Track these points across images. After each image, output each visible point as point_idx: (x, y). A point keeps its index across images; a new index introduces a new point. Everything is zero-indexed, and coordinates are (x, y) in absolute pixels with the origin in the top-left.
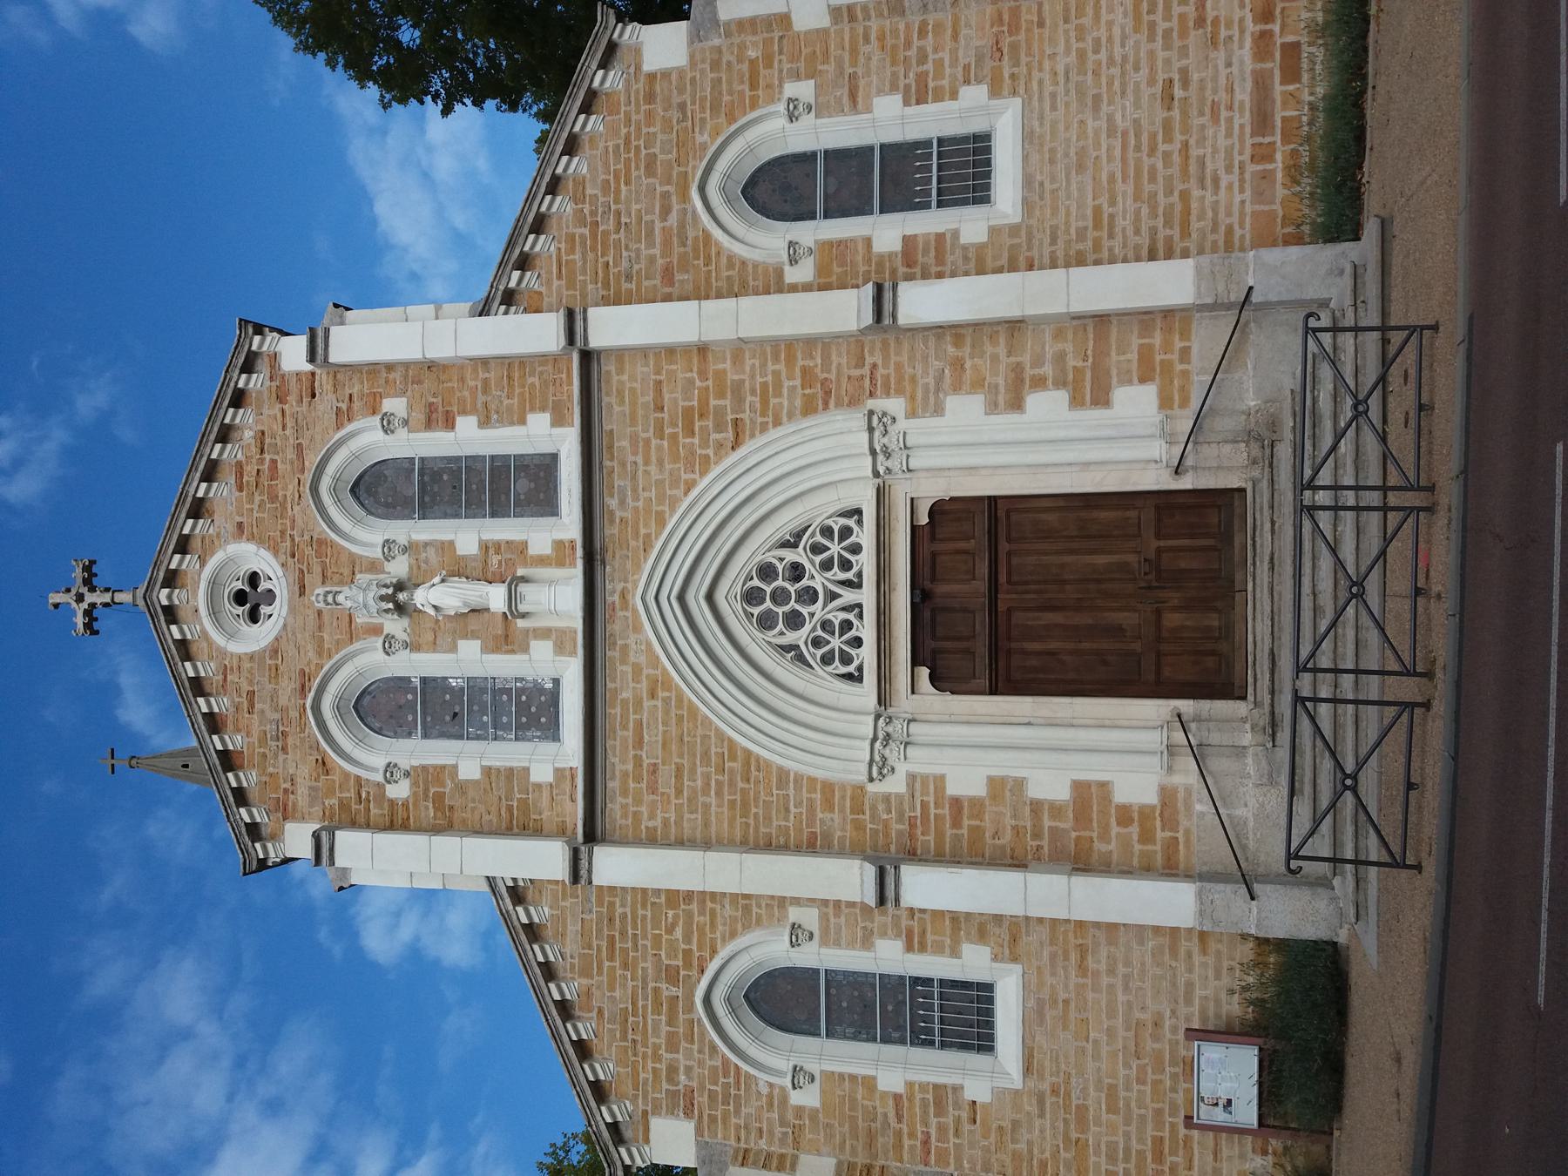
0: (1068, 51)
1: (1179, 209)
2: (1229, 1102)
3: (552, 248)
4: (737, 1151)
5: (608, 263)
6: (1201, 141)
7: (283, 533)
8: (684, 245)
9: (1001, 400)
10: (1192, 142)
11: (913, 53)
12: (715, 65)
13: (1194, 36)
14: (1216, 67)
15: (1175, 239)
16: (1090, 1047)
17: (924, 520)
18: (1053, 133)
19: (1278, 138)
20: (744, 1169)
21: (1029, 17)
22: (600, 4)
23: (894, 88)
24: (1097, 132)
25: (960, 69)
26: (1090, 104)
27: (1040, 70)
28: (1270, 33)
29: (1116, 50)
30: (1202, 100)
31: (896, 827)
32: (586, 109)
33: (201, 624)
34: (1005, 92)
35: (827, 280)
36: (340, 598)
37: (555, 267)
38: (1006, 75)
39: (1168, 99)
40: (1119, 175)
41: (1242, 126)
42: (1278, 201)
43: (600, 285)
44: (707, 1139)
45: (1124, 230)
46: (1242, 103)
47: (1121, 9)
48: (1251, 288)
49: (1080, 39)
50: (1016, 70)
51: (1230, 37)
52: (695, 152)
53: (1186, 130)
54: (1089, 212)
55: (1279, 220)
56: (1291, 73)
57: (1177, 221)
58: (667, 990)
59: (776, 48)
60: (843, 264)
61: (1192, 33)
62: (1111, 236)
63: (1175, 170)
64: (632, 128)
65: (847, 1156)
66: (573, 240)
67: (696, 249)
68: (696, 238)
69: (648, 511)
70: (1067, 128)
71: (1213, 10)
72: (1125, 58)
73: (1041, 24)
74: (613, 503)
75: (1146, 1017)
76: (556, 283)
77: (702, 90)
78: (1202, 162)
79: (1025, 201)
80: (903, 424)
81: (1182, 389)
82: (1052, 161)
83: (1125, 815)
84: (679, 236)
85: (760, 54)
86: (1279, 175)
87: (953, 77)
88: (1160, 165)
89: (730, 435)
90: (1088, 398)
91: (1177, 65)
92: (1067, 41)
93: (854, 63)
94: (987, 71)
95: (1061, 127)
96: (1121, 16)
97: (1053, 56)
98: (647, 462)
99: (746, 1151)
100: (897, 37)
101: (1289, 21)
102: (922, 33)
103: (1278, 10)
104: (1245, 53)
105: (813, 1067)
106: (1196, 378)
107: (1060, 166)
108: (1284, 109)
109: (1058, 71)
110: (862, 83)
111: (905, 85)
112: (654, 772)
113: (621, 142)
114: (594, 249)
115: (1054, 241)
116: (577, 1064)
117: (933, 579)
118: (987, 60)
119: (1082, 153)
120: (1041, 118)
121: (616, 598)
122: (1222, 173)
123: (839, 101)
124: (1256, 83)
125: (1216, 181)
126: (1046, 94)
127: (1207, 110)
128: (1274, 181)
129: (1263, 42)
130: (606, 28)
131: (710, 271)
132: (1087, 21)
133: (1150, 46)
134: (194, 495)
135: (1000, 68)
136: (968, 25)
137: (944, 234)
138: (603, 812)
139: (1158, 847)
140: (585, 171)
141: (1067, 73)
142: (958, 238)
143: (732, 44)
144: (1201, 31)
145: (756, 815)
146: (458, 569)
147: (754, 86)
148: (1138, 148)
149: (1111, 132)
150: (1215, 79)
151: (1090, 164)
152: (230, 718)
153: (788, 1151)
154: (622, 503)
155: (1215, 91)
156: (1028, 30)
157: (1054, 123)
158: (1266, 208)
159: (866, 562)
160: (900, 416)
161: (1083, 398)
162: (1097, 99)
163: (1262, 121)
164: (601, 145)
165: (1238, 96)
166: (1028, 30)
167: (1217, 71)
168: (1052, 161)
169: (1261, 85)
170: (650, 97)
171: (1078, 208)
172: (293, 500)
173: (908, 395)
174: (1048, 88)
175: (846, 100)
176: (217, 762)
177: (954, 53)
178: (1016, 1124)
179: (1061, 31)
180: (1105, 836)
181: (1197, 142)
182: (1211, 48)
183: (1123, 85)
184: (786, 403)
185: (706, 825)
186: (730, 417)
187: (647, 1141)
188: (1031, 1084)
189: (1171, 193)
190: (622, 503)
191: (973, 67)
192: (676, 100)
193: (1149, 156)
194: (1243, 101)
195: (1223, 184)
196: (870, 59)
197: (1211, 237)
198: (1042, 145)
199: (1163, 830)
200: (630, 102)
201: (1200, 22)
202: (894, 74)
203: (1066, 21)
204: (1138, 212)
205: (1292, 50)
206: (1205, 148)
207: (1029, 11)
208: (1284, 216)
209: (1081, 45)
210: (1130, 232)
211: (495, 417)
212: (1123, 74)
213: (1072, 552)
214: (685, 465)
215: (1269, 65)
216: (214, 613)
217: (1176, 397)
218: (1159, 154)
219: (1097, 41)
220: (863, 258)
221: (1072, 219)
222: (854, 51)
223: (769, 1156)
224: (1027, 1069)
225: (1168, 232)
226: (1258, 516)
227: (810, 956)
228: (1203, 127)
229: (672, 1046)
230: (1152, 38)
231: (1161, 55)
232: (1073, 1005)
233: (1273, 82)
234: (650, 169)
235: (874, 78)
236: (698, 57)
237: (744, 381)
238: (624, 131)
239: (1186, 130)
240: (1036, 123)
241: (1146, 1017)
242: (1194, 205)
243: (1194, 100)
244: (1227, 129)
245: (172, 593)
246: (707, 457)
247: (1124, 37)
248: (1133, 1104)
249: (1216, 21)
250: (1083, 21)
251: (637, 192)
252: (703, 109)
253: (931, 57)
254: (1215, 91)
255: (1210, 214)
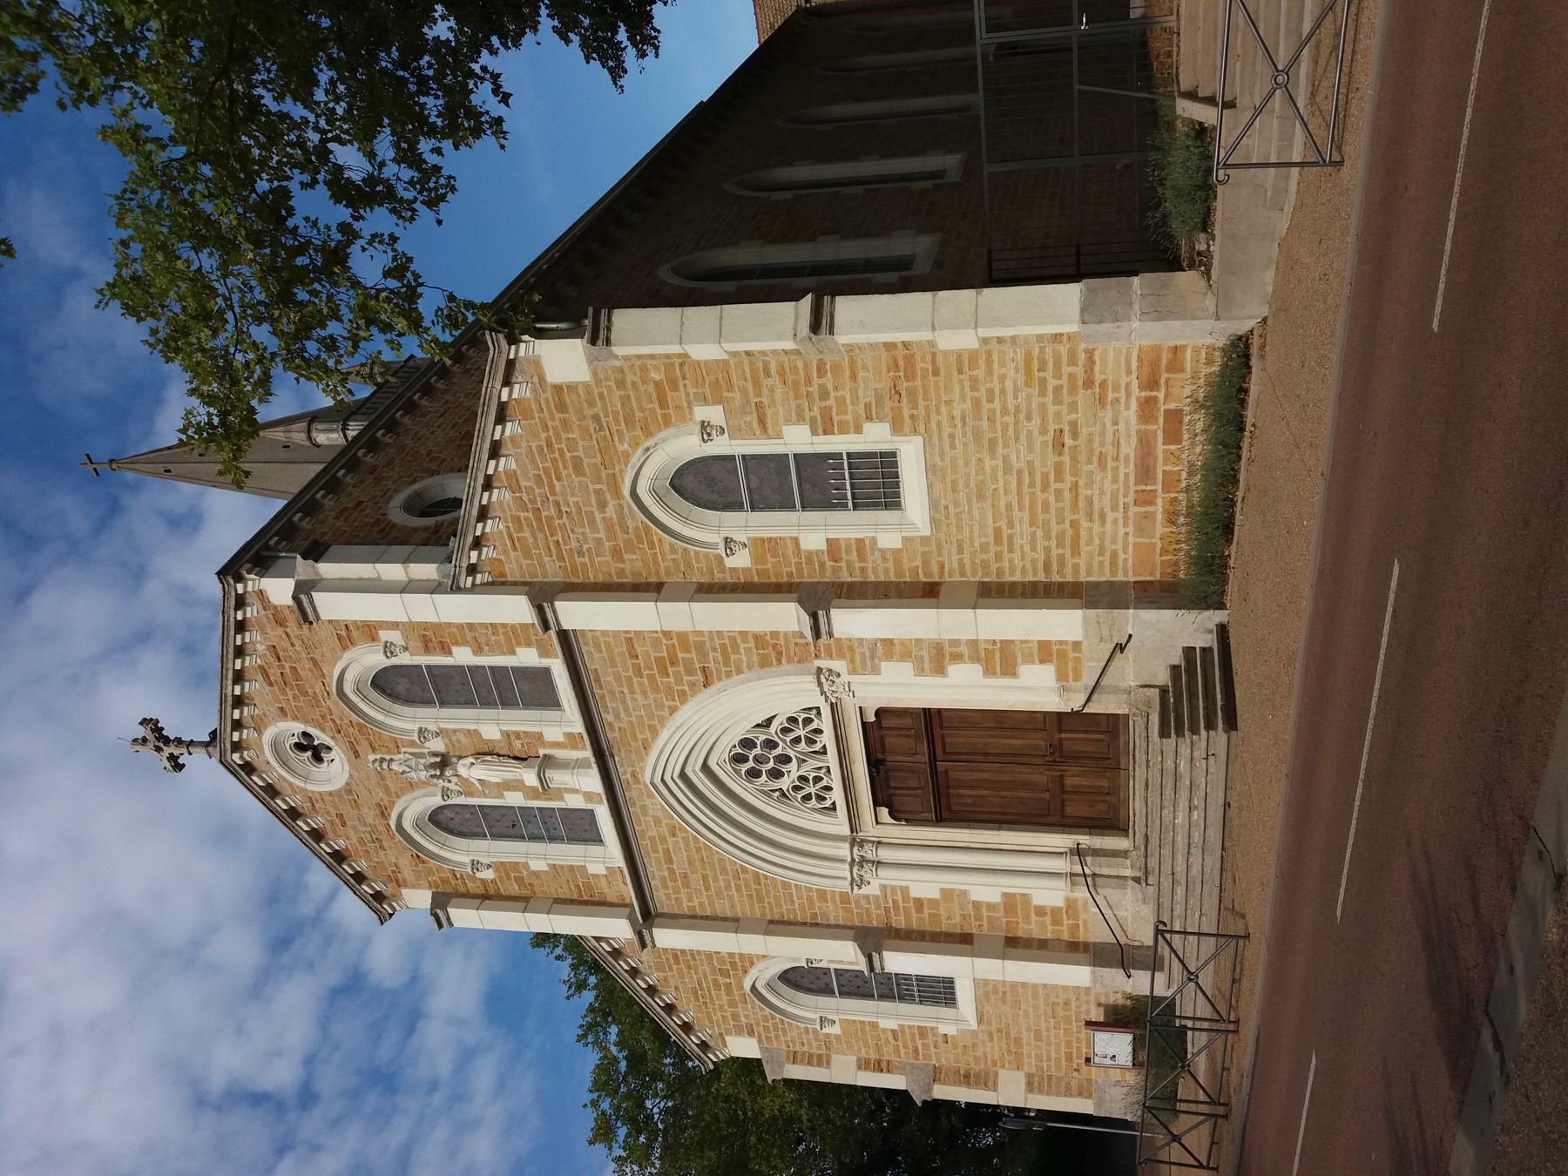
0: (963, 398)
1: (1070, 533)
2: (1114, 1056)
3: (501, 526)
4: (789, 1052)
5: (558, 541)
6: (1090, 484)
7: (323, 717)
8: (627, 533)
9: (926, 666)
10: (1081, 482)
11: (814, 389)
12: (621, 384)
13: (1083, 396)
14: (1104, 424)
15: (1066, 556)
16: (1021, 1013)
17: (872, 718)
18: (954, 468)
19: (1159, 487)
20: (796, 1066)
21: (924, 365)
22: (487, 332)
23: (800, 419)
24: (994, 469)
25: (862, 406)
26: (986, 445)
27: (938, 413)
28: (1155, 399)
29: (1009, 401)
30: (1091, 451)
31: (874, 912)
32: (501, 419)
33: (276, 772)
34: (907, 430)
35: (764, 567)
36: (394, 766)
37: (508, 541)
38: (906, 416)
39: (1059, 445)
40: (1015, 505)
41: (1126, 475)
42: (1158, 535)
43: (554, 558)
44: (766, 1045)
45: (1022, 547)
46: (1127, 456)
47: (1013, 365)
48: (1130, 636)
49: (973, 388)
50: (915, 412)
51: (1117, 400)
52: (619, 458)
53: (1075, 472)
54: (990, 532)
55: (1158, 550)
56: (1172, 435)
57: (1068, 543)
58: (722, 980)
59: (678, 372)
60: (776, 556)
61: (1081, 391)
62: (1011, 550)
63: (1066, 504)
64: (551, 433)
65: (863, 1054)
66: (520, 522)
67: (638, 537)
68: (637, 528)
69: (641, 724)
70: (966, 464)
71: (1101, 374)
72: (1017, 409)
73: (936, 373)
74: (609, 717)
75: (1060, 1000)
76: (513, 554)
77: (614, 405)
78: (1090, 500)
79: (933, 520)
80: (845, 678)
81: (1075, 669)
82: (954, 490)
83: (1041, 911)
84: (620, 526)
85: (663, 376)
86: (1159, 517)
87: (857, 416)
88: (1052, 499)
89: (701, 678)
90: (998, 669)
91: (1067, 418)
92: (962, 390)
93: (759, 393)
94: (887, 410)
95: (961, 463)
96: (1013, 371)
97: (949, 403)
98: (632, 692)
99: (795, 1052)
100: (797, 374)
101: (1172, 390)
102: (821, 371)
103: (1163, 380)
104: (1131, 414)
105: (740, 537)
106: (1086, 664)
107: (962, 495)
108: (1164, 465)
109: (955, 415)
110: (769, 412)
111: (811, 417)
112: (685, 877)
113: (543, 443)
114: (541, 530)
115: (960, 551)
116: (667, 1018)
117: (884, 752)
118: (887, 401)
119: (981, 485)
120: (942, 454)
121: (628, 776)
122: (1107, 510)
123: (749, 424)
124: (1141, 441)
125: (1103, 517)
126: (945, 435)
127: (1095, 459)
128: (1154, 522)
129: (1147, 408)
130: (500, 352)
131: (655, 554)
132: (980, 373)
133: (1042, 400)
134: (233, 695)
135: (900, 408)
136: (865, 368)
137: (863, 540)
138: (652, 899)
139: (1065, 928)
140: (514, 466)
141: (963, 418)
142: (876, 544)
143: (633, 365)
144: (1089, 391)
145: (769, 903)
146: (486, 752)
147: (663, 404)
148: (1032, 485)
149: (1007, 469)
150: (1103, 433)
151: (989, 494)
152: (329, 830)
153: (824, 1052)
154: (617, 717)
155: (1102, 444)
156: (924, 377)
157: (954, 460)
158: (1147, 541)
159: (827, 738)
160: (844, 673)
161: (995, 669)
162: (993, 443)
163: (1145, 472)
164: (524, 445)
165: (1124, 450)
166: (924, 377)
167: (1105, 426)
168: (954, 490)
169: (1145, 443)
170: (562, 407)
171: (980, 528)
172: (323, 695)
173: (848, 659)
174: (947, 430)
175: (755, 425)
176: (332, 861)
177: (854, 391)
178: (974, 1045)
179: (955, 381)
180: (1027, 919)
181: (1086, 485)
182: (1099, 407)
183: (1017, 431)
184: (744, 658)
185: (733, 906)
186: (697, 666)
187: (726, 1046)
188: (983, 1027)
189: (1063, 521)
190: (617, 717)
191: (874, 406)
192: (589, 412)
193: (1043, 492)
194: (1129, 454)
195: (1109, 519)
196: (773, 391)
197: (1098, 559)
198: (944, 476)
199: (1068, 919)
200: (542, 409)
201: (1089, 383)
202: (798, 406)
203: (960, 372)
204: (1033, 535)
205: (1174, 417)
206: (1092, 490)
207: (923, 360)
208: (1162, 548)
209: (975, 394)
210: (1027, 548)
211: (487, 648)
212: (1017, 422)
213: (992, 737)
214: (666, 696)
215: (1153, 427)
216: (284, 763)
217: (1071, 674)
218: (1051, 490)
219: (991, 392)
220: (794, 553)
221: (976, 534)
222: (757, 383)
223: (811, 1055)
224: (980, 1020)
225: (1061, 551)
226: (1137, 740)
227: (720, 446)
228: (1091, 473)
229: (732, 1004)
230: (1042, 393)
231: (1052, 408)
232: (1009, 994)
233: (1156, 441)
234: (578, 467)
235: (780, 408)
236: (601, 375)
237: (705, 642)
238: (544, 435)
239: (1075, 472)
240: (937, 459)
241: (1060, 1000)
242: (1083, 533)
243: (1083, 449)
244: (1113, 476)
245: (242, 753)
246: (683, 692)
247: (1016, 391)
248: (1052, 1038)
249: (1103, 384)
250: (976, 372)
251: (570, 487)
252: (617, 422)
253: (832, 394)
254: (1102, 444)
255: (1097, 541)
